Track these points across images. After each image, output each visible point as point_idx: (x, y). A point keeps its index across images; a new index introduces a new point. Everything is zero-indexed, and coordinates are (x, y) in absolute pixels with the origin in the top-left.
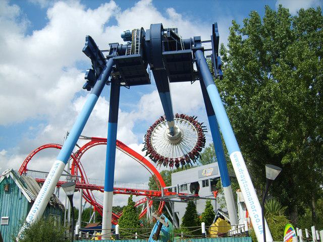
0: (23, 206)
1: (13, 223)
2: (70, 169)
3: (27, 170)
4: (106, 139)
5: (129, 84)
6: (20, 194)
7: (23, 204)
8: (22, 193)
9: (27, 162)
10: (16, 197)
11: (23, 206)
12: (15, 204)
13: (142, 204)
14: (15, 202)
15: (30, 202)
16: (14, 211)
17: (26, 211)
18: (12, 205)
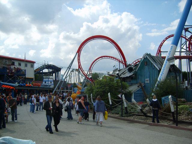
0: (155, 72)
1: (151, 82)
2: (188, 48)
3: (161, 52)
4: (32, 79)
5: (172, 22)
6: (153, 66)
7: (155, 71)
8: (154, 66)
9: (161, 47)
10: (151, 68)
11: (155, 72)
12: (151, 72)
13: (138, 63)
14: (151, 71)
15: (159, 70)
16: (151, 75)
17: (157, 73)
18: (150, 73)
